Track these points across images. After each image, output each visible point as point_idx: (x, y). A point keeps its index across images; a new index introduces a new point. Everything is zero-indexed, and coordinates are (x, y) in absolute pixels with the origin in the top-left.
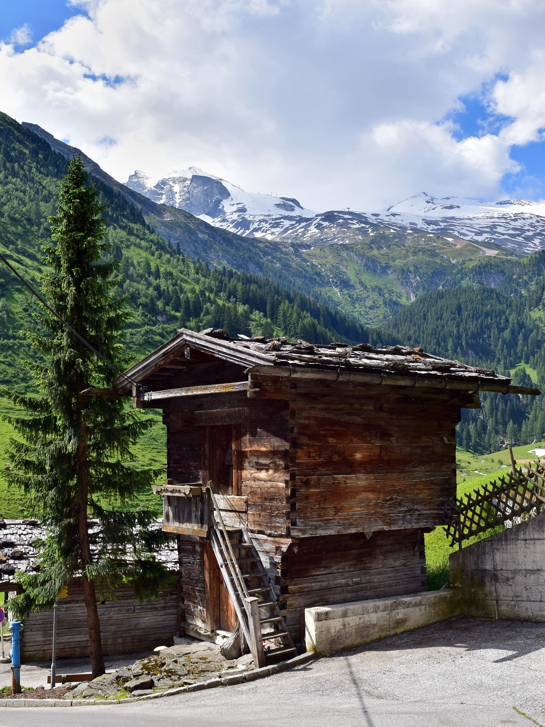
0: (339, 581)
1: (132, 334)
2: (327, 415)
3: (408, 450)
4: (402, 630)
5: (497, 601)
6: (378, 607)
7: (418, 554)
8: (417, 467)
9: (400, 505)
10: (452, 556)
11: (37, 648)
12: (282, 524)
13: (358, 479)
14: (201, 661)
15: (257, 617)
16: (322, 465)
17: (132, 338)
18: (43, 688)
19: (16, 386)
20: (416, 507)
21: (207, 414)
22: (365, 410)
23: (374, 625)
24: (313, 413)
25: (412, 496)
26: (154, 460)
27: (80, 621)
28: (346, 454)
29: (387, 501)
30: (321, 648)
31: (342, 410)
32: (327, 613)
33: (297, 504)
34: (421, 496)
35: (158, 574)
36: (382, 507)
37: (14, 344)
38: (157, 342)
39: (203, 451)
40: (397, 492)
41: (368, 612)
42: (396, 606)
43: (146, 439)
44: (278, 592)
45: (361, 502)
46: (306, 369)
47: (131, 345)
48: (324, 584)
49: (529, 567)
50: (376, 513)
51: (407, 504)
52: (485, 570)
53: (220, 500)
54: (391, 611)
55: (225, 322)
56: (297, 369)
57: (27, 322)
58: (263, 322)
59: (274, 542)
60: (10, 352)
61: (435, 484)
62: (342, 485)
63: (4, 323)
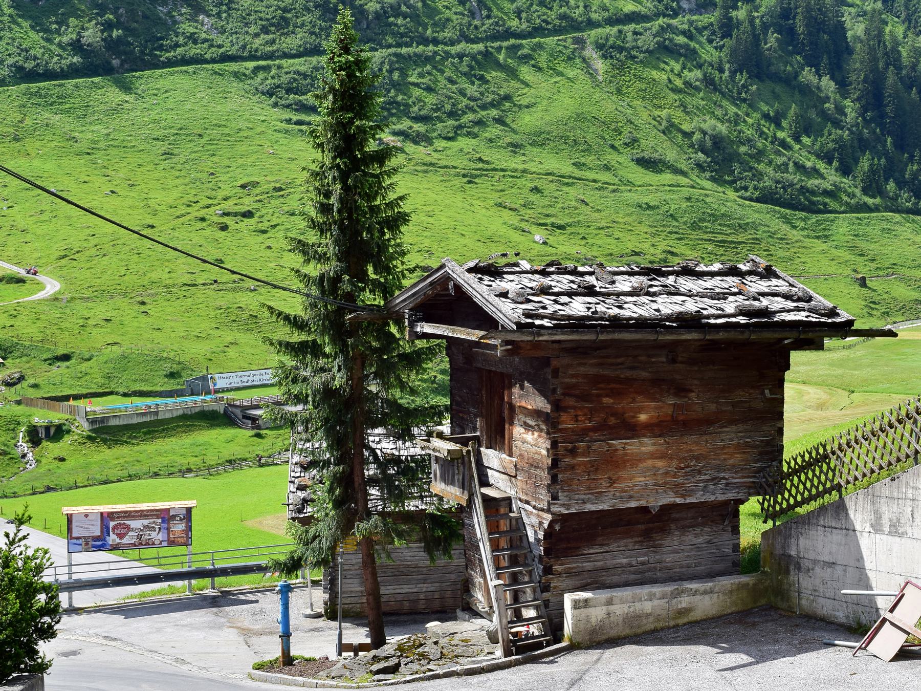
0: (619, 561)
1: (635, 33)
2: (601, 372)
3: (713, 407)
4: (685, 620)
5: (799, 593)
6: (655, 594)
7: (730, 528)
8: (726, 426)
9: (700, 473)
10: (765, 534)
11: (353, 600)
12: (544, 497)
13: (641, 444)
14: (463, 644)
15: (502, 602)
16: (594, 429)
17: (636, 40)
18: (327, 659)
19: (440, 125)
20: (722, 475)
21: (483, 354)
22: (653, 363)
23: (648, 615)
24: (582, 370)
25: (718, 462)
26: (672, 253)
27: (409, 566)
28: (626, 415)
29: (683, 468)
30: (579, 639)
31: (622, 364)
32: (586, 601)
33: (560, 476)
34: (731, 462)
35: (447, 532)
36: (675, 476)
37: (436, 53)
38: (680, 46)
39: (479, 397)
40: (697, 458)
41: (640, 600)
42: (678, 594)
43: (658, 217)
44: (540, 572)
45: (647, 471)
46: (554, 331)
47: (634, 53)
48: (599, 564)
49: (826, 559)
50: (666, 483)
51: (710, 472)
52: (790, 556)
53: (492, 457)
54: (671, 599)
55: (799, 10)
56: (542, 331)
57: (456, 13)
58: (869, 8)
59: (538, 516)
60: (429, 67)
61: (752, 447)
62: (620, 452)
63: (418, 16)
